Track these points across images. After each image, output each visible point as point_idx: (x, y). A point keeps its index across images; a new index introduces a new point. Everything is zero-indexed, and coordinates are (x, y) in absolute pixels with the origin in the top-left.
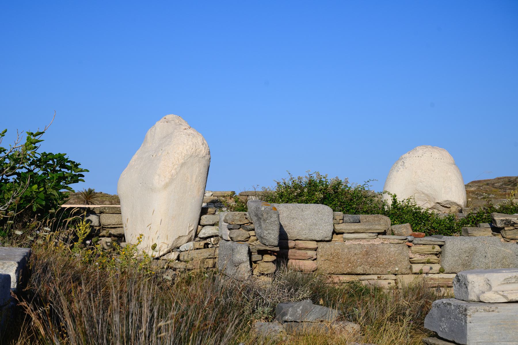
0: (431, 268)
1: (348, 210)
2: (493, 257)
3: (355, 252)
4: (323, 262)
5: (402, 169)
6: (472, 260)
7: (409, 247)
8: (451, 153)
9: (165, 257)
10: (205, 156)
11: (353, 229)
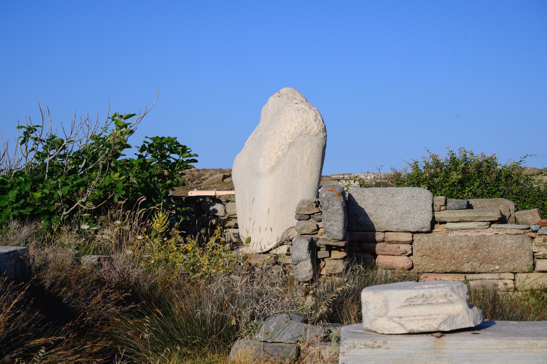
1: (495, 192)
3: (460, 246)
7: (533, 238)
9: (274, 251)
10: (318, 134)
11: (457, 218)
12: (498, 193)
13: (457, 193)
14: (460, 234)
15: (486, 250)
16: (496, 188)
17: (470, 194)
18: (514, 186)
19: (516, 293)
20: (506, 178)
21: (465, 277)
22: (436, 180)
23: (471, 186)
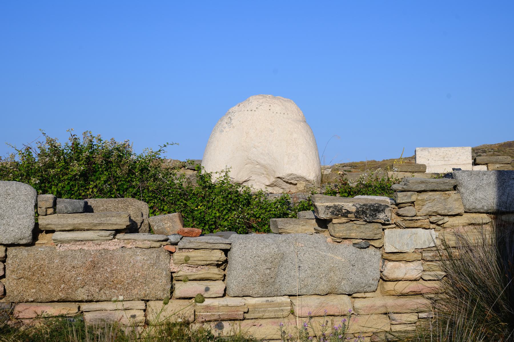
0: (207, 289)
1: (127, 189)
2: (312, 269)
3: (73, 264)
4: (15, 281)
5: (227, 129)
6: (277, 275)
7: (171, 253)
8: (299, 104)
11: (70, 225)
12: (131, 189)
13: (78, 189)
14: (74, 247)
15: (109, 270)
16: (129, 184)
17: (95, 190)
18: (151, 182)
19: (148, 329)
20: (142, 170)
21: (79, 308)
22: (52, 172)
23: (97, 180)
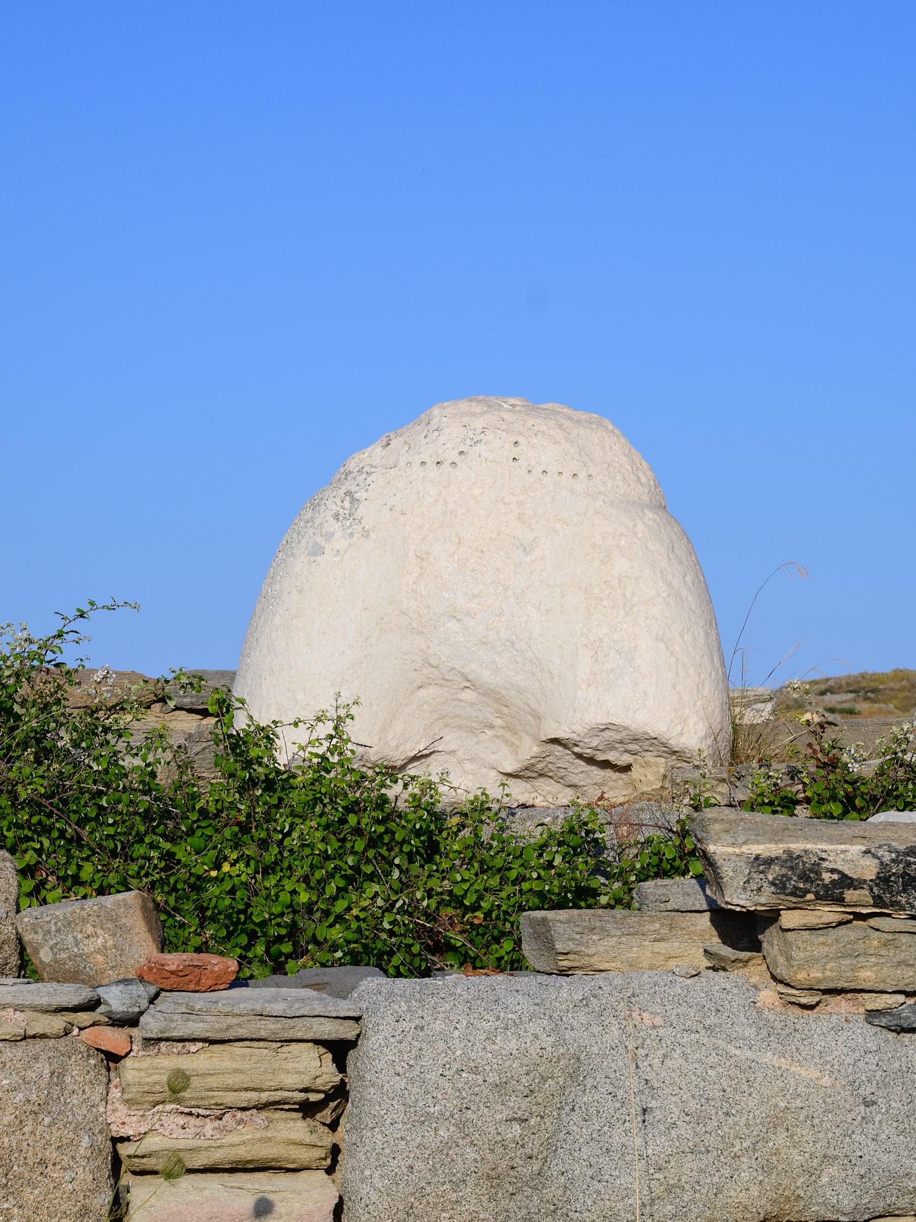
2: (700, 1119)
6: (551, 1146)
7: (112, 1059)
8: (639, 439)
